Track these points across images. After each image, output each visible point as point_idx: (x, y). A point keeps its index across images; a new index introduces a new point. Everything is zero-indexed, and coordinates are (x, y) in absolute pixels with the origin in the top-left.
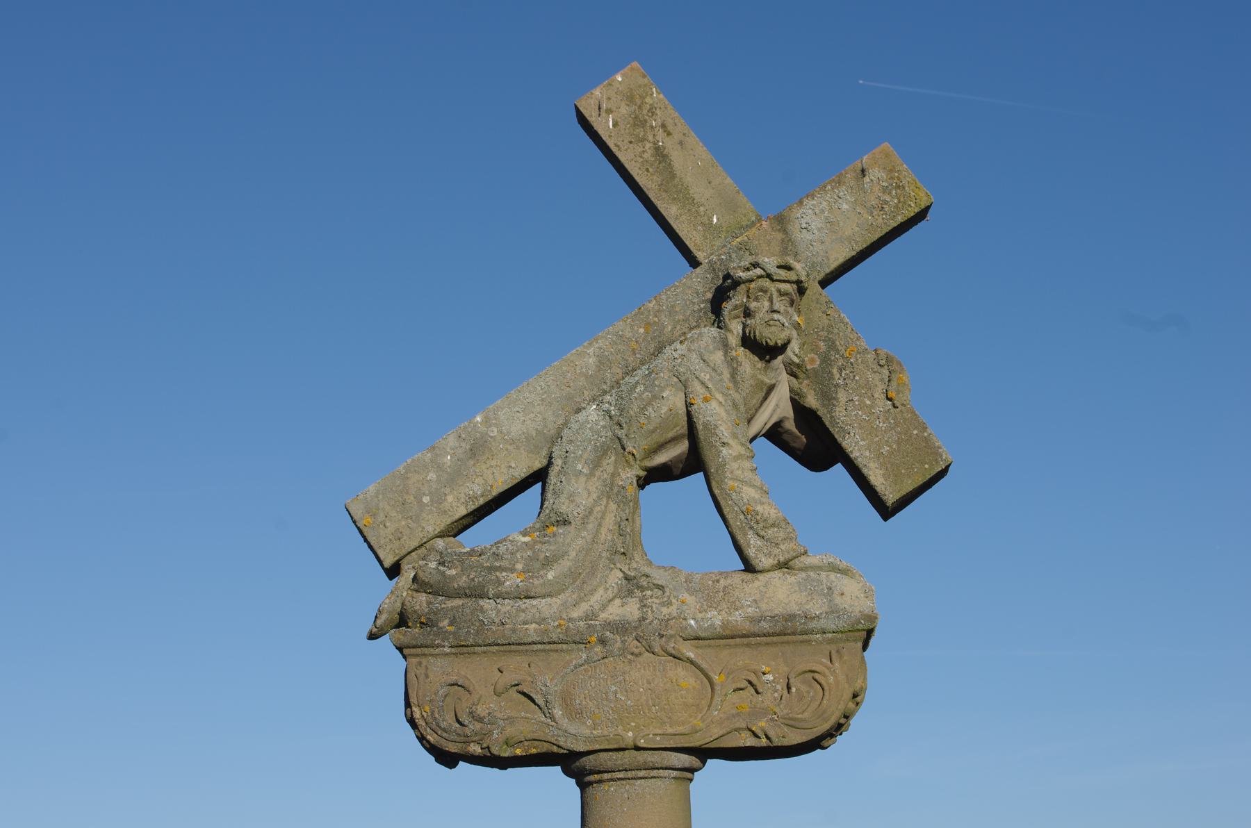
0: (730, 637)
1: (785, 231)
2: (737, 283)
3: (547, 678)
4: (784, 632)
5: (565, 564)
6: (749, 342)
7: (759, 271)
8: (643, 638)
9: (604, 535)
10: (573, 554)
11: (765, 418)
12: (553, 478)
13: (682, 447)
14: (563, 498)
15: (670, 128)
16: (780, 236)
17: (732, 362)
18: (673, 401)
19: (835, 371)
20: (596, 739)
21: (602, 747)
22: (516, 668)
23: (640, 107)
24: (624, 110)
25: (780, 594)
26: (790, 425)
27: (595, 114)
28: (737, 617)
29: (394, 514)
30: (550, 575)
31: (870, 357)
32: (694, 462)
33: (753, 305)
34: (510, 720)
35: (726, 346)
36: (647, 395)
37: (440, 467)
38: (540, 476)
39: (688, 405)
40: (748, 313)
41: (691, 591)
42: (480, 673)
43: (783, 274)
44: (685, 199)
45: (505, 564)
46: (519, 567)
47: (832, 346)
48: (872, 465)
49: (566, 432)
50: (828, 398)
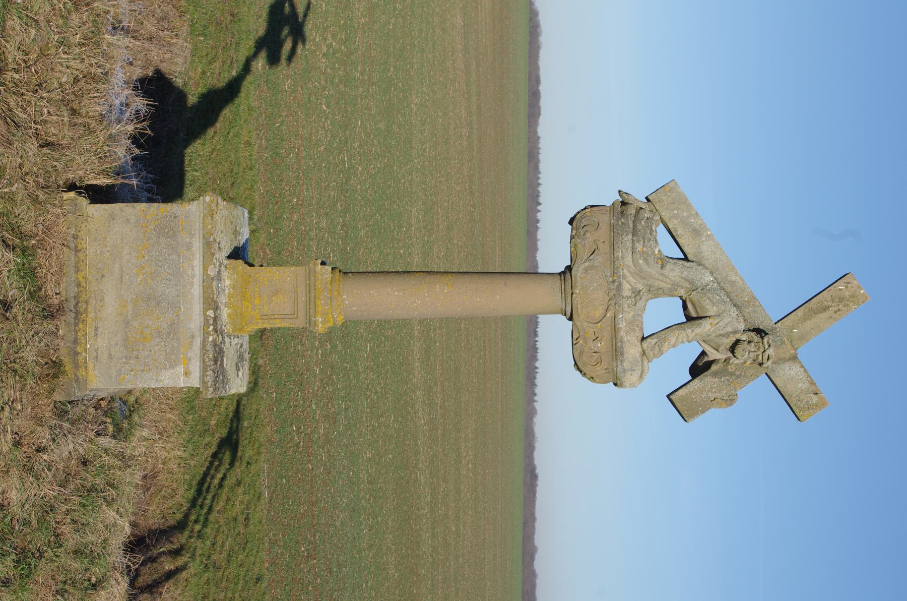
0: (615, 330)
1: (789, 359)
2: (762, 338)
3: (598, 260)
4: (617, 351)
5: (645, 267)
6: (738, 342)
7: (767, 347)
8: (615, 296)
9: (657, 283)
11: (708, 349)
12: (685, 263)
13: (694, 314)
14: (672, 266)
16: (787, 357)
17: (727, 335)
18: (712, 310)
20: (576, 278)
22: (605, 248)
24: (847, 294)
25: (632, 350)
26: (706, 359)
28: (622, 334)
30: (641, 261)
31: (733, 392)
32: (689, 318)
33: (753, 344)
34: (584, 246)
35: (735, 332)
36: (715, 300)
37: (689, 217)
38: (686, 259)
39: (710, 317)
40: (750, 342)
41: (634, 316)
42: (603, 234)
43: (766, 357)
44: (805, 318)
47: (738, 377)
49: (700, 268)
50: (715, 374)
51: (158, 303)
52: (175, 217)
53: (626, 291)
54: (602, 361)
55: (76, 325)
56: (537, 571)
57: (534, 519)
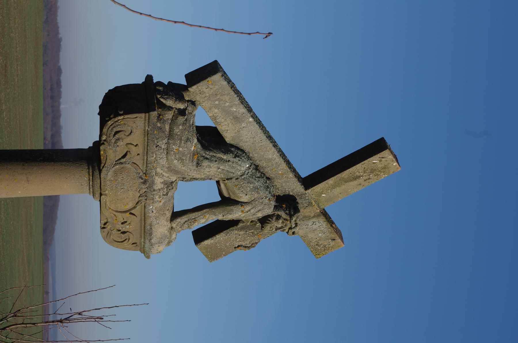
1: (314, 217)
4: (146, 232)
7: (294, 226)
10: (184, 168)
15: (368, 181)
16: (312, 215)
19: (252, 231)
21: (102, 182)
23: (380, 171)
27: (381, 156)
29: (212, 91)
37: (231, 107)
45: (183, 144)
46: (181, 149)
48: (212, 241)
50: (242, 229)
54: (129, 233)
56: (62, 68)
57: (59, 95)
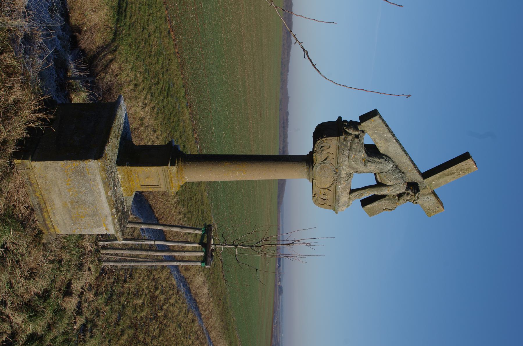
4: (336, 200)
50: (388, 199)
51: (84, 203)
52: (83, 168)
53: (343, 174)
54: (327, 199)
55: (42, 214)
